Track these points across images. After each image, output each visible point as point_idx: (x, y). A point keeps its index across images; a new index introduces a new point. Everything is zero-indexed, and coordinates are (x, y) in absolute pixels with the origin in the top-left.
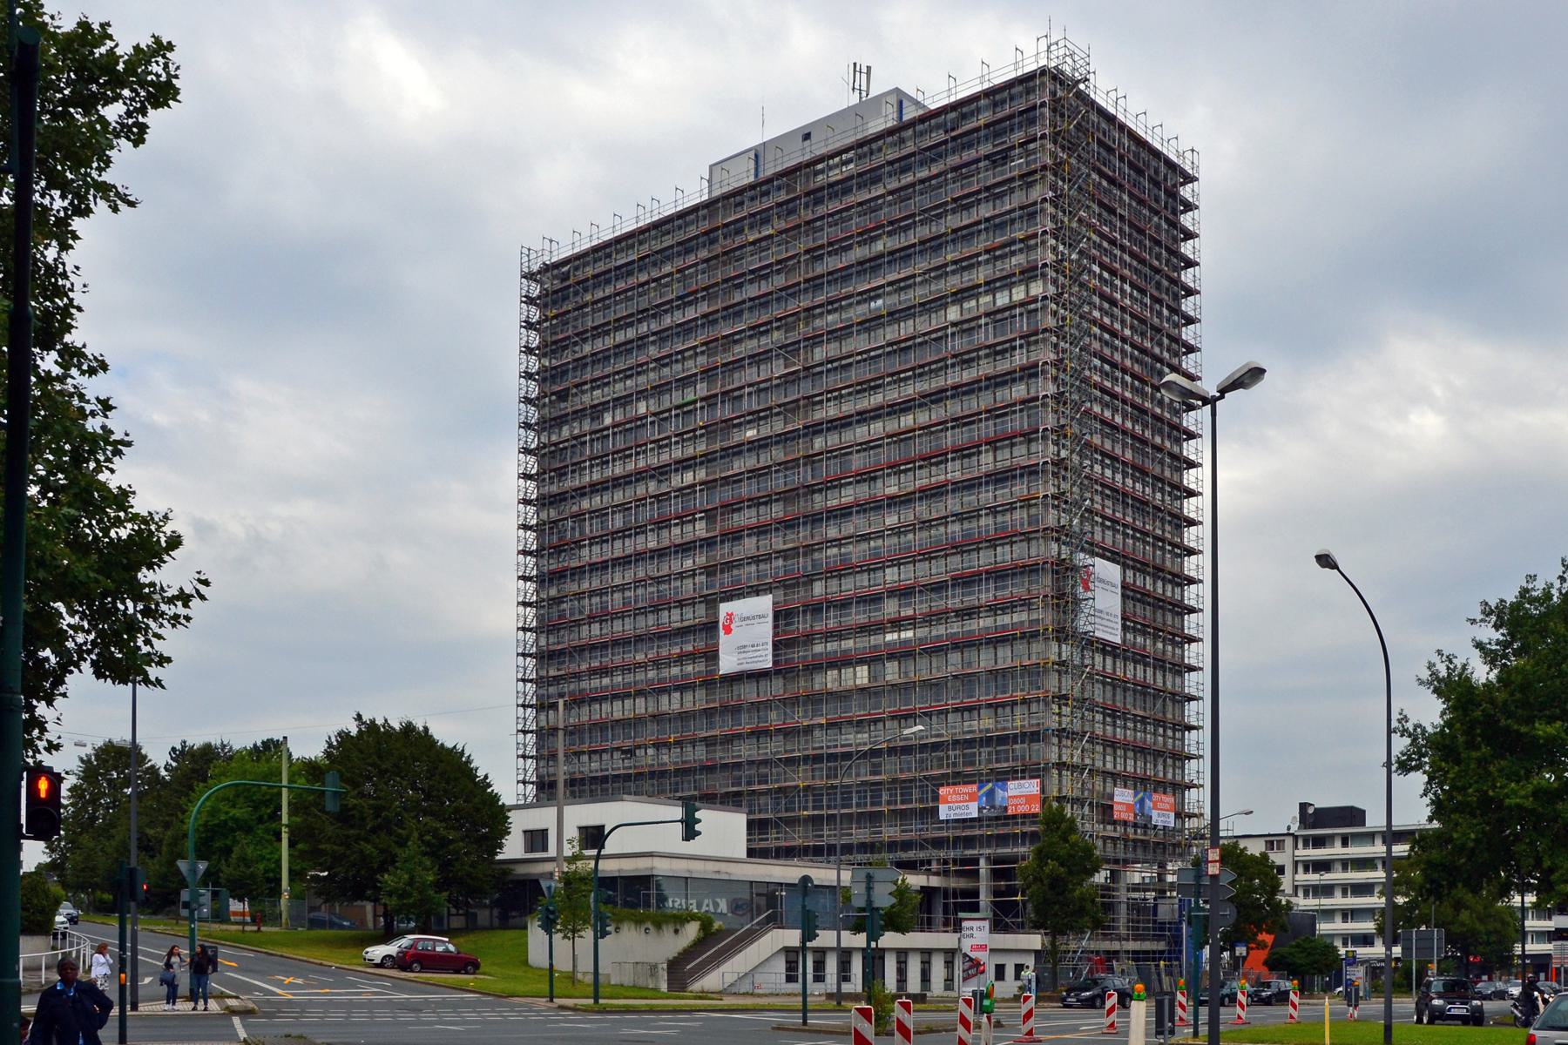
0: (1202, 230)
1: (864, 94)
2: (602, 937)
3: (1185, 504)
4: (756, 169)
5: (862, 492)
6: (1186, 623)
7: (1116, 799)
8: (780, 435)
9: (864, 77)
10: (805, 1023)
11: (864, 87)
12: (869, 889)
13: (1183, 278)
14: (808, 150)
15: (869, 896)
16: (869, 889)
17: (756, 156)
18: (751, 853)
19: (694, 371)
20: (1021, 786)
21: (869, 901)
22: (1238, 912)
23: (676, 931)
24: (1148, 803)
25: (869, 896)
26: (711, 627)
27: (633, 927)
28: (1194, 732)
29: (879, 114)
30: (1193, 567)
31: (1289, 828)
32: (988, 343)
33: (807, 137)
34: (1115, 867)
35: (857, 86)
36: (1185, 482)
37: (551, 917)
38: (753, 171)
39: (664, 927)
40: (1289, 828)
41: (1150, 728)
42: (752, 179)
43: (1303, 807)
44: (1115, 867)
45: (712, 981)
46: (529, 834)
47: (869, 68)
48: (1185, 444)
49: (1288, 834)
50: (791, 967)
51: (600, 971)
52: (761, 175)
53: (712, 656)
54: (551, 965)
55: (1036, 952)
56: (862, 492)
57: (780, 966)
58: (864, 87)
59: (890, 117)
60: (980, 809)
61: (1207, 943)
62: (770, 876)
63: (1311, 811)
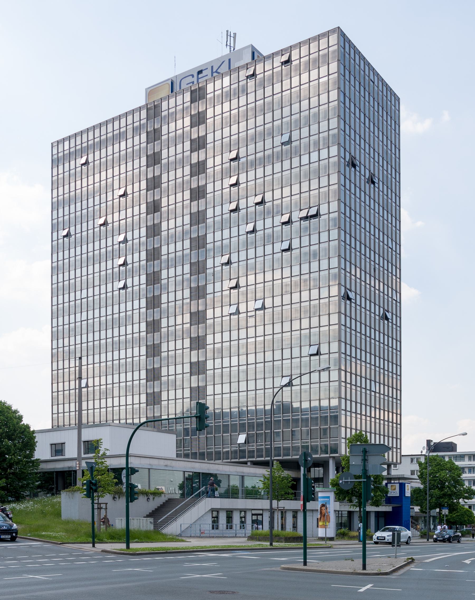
1: (232, 49)
2: (131, 501)
9: (232, 39)
11: (232, 45)
12: (365, 460)
15: (365, 466)
16: (365, 460)
17: (172, 83)
18: (178, 455)
21: (365, 471)
22: (281, 500)
25: (365, 466)
31: (422, 452)
33: (200, 72)
35: (228, 44)
37: (94, 488)
40: (422, 452)
43: (429, 442)
47: (235, 34)
49: (421, 455)
50: (215, 521)
57: (209, 520)
58: (232, 45)
62: (193, 468)
63: (432, 444)
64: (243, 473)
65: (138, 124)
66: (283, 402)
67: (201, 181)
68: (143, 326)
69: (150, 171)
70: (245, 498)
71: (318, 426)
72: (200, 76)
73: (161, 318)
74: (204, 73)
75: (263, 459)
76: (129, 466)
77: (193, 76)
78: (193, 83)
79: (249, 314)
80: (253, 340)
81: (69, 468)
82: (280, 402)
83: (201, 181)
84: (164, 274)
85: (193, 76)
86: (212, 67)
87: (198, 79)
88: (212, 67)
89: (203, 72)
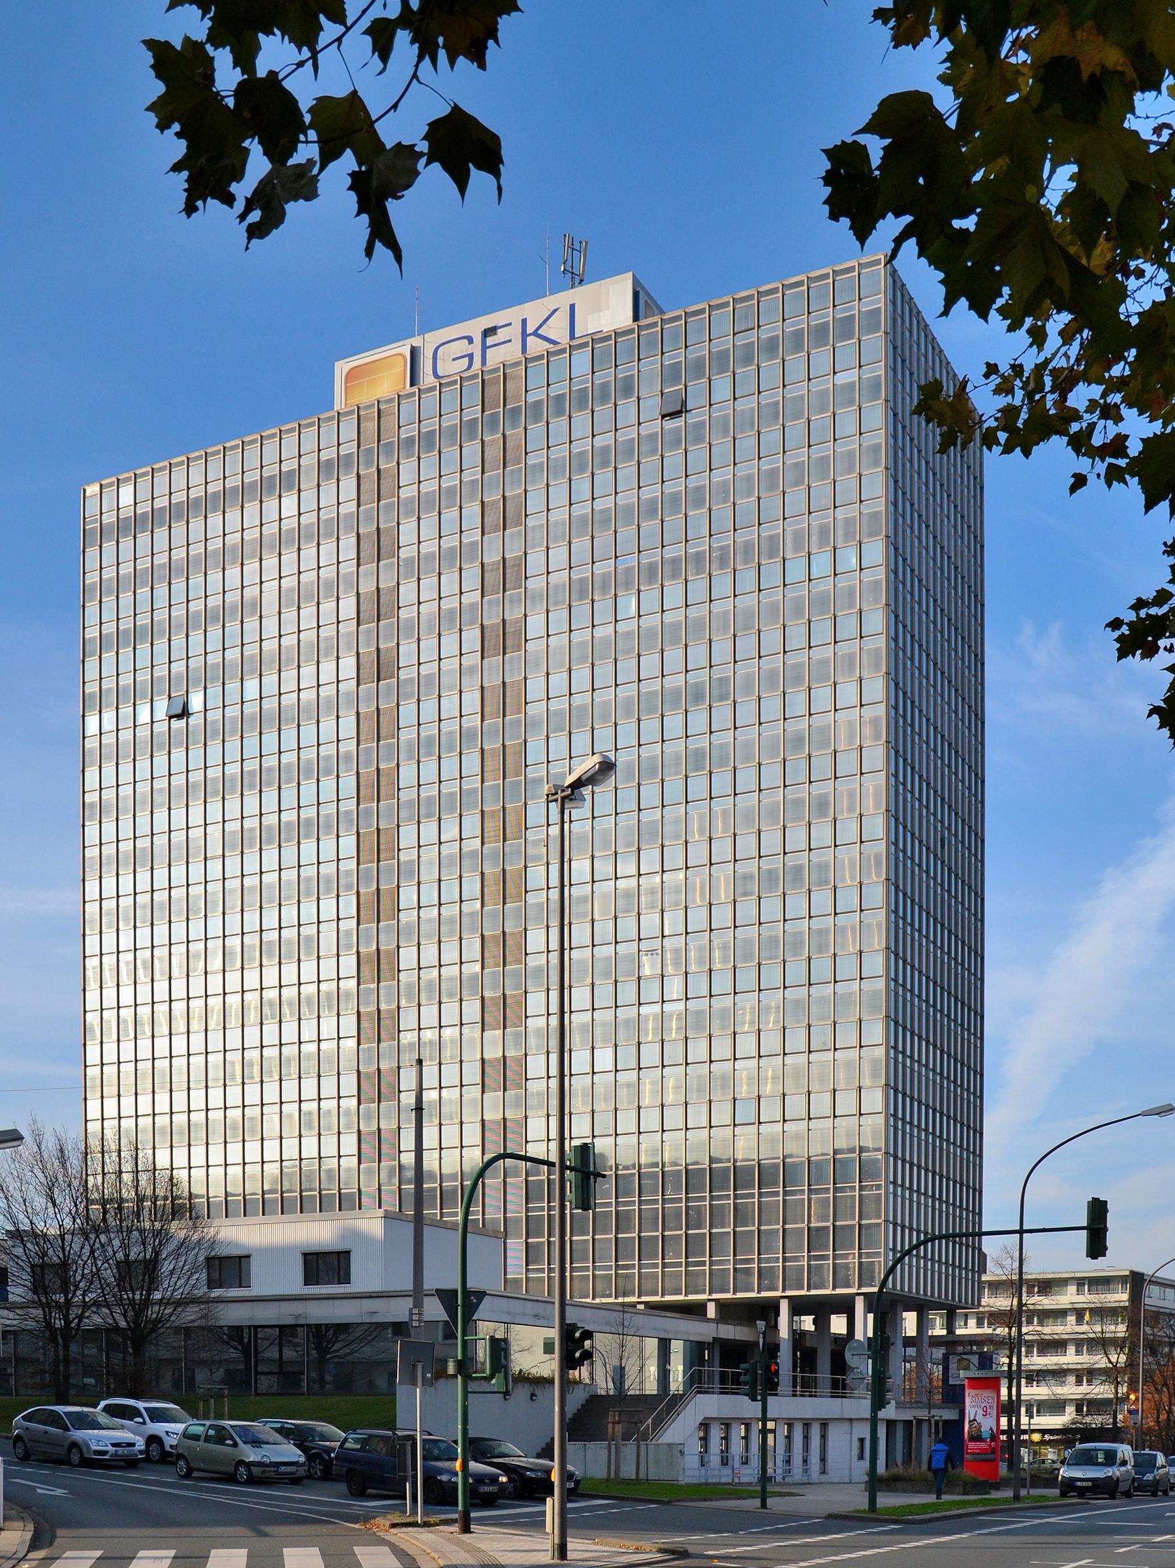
64: (666, 1331)
65: (752, 403)
66: (735, 1161)
67: (512, 608)
68: (349, 963)
69: (366, 575)
70: (721, 1393)
71: (828, 1221)
72: (490, 341)
73: (398, 947)
74: (502, 335)
75: (681, 1298)
76: (1025, 1277)
77: (470, 340)
78: (471, 356)
79: (644, 945)
80: (587, 1017)
81: (297, 1317)
82: (240, 1195)
83: (512, 608)
84: (408, 835)
85: (470, 340)
86: (524, 321)
87: (484, 348)
88: (524, 321)
89: (499, 331)
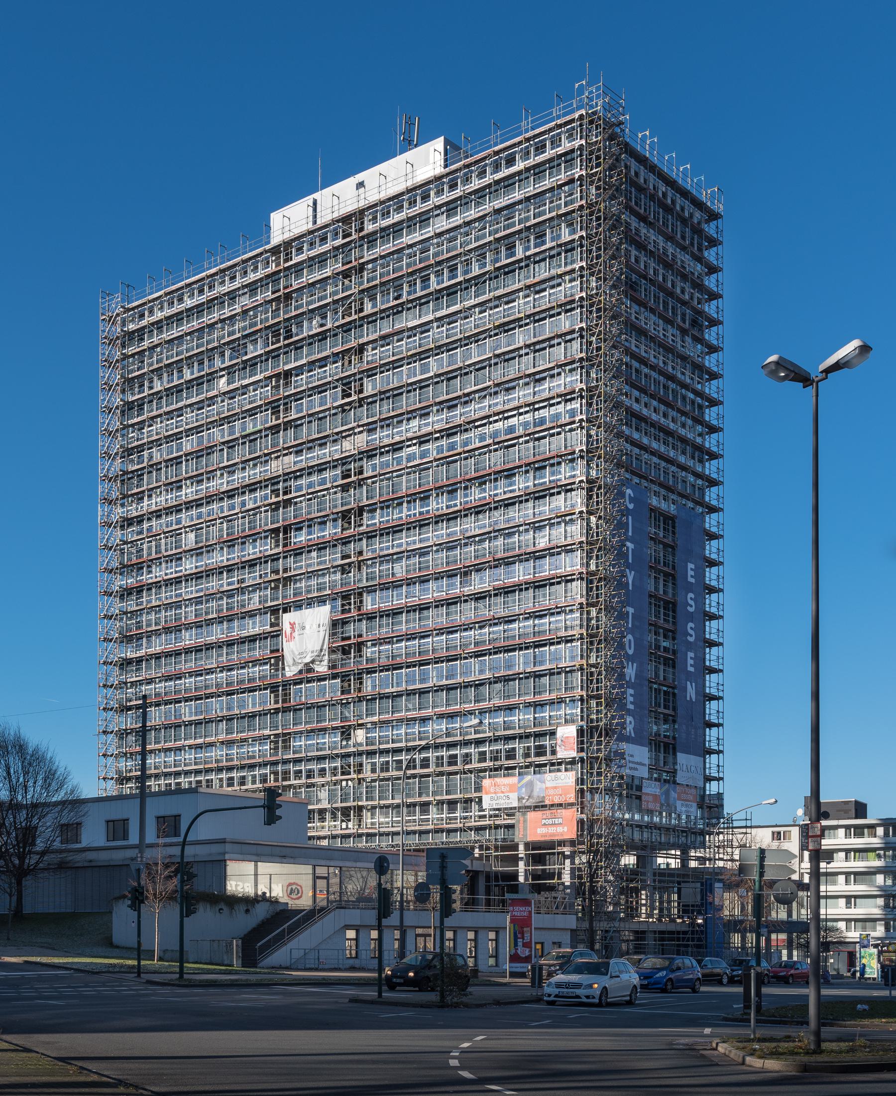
0: (726, 318)
2: (187, 916)
3: (707, 519)
4: (315, 217)
5: (416, 510)
6: (707, 629)
7: (644, 790)
8: (337, 460)
10: (380, 995)
13: (707, 336)
14: (362, 196)
19: (259, 403)
20: (556, 778)
23: (247, 911)
24: (673, 795)
26: (276, 635)
27: (208, 906)
28: (714, 730)
29: (426, 163)
30: (714, 577)
32: (528, 372)
34: (642, 853)
36: (707, 499)
38: (311, 218)
39: (236, 908)
41: (721, 850)
42: (310, 226)
44: (642, 853)
45: (279, 956)
46: (111, 824)
48: (707, 464)
51: (185, 949)
52: (319, 222)
53: (277, 659)
54: (139, 943)
55: (572, 930)
56: (416, 510)
59: (438, 163)
60: (520, 799)
61: (790, 879)
